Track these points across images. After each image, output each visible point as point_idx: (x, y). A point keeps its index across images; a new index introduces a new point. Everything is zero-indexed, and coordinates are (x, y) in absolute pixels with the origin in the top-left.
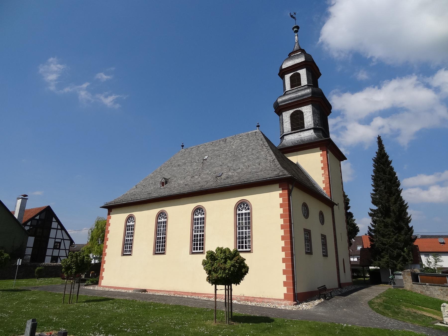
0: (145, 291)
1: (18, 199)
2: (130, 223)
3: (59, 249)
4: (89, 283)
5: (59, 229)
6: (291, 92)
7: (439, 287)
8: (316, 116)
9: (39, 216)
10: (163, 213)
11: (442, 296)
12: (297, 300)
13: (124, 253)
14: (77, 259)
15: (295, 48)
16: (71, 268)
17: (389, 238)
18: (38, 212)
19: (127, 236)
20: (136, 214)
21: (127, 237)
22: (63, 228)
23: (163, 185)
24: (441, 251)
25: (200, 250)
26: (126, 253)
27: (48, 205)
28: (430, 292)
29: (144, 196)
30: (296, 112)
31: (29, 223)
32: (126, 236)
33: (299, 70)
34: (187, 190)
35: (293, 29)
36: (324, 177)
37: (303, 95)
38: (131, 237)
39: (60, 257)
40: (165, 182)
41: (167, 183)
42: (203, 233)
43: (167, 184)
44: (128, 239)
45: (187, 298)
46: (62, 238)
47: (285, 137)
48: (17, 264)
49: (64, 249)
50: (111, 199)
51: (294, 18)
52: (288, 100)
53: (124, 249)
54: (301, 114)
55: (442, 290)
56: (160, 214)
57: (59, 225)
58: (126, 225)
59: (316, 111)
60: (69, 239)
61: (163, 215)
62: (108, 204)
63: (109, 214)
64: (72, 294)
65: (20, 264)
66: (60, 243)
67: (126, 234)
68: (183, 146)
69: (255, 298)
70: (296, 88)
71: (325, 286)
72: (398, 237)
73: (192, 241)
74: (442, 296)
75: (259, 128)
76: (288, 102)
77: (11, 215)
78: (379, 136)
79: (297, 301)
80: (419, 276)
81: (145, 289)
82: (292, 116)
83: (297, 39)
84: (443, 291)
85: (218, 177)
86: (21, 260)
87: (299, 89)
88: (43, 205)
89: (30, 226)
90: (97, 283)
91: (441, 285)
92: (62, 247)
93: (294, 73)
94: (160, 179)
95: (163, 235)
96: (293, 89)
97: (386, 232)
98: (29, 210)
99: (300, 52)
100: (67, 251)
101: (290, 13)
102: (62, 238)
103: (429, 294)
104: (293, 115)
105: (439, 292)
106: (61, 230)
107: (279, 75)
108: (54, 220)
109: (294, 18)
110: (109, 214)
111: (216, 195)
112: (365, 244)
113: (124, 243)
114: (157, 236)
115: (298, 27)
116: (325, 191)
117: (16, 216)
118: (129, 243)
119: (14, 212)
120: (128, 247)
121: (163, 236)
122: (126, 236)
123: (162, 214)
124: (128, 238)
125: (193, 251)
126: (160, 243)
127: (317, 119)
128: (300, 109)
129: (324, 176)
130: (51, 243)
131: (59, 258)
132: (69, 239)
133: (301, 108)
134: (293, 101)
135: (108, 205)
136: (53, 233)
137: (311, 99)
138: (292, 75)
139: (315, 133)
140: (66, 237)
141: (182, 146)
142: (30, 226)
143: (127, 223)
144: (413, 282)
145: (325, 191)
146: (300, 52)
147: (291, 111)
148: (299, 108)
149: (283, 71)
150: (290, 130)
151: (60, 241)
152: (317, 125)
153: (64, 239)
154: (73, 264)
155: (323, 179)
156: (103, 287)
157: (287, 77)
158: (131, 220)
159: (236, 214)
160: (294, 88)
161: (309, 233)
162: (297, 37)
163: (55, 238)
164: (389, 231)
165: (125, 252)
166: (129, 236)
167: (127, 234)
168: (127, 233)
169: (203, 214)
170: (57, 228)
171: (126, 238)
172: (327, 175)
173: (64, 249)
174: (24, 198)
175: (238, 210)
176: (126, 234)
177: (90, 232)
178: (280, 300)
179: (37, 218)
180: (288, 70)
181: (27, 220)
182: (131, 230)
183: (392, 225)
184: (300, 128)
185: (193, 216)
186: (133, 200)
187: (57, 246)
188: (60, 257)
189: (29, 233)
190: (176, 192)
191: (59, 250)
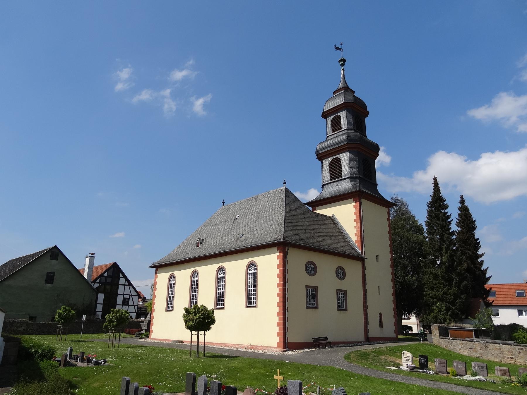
0: (182, 342)
1: (87, 258)
2: (252, 271)
3: (128, 305)
4: (143, 336)
5: (127, 285)
6: (332, 137)
7: (459, 341)
9: (107, 272)
10: (253, 263)
11: (463, 350)
12: (287, 348)
13: (168, 309)
14: (116, 314)
16: (113, 322)
17: (437, 291)
18: (107, 268)
19: (219, 288)
20: (177, 273)
21: (219, 290)
22: (130, 284)
23: (198, 246)
24: (502, 304)
25: (253, 304)
26: (169, 309)
27: (111, 262)
28: (453, 346)
29: (181, 258)
30: (333, 161)
31: (98, 281)
34: (218, 250)
35: (339, 62)
36: (356, 230)
37: (339, 142)
38: (223, 290)
40: (200, 242)
41: (202, 244)
42: (223, 291)
43: (202, 245)
44: (220, 292)
47: (326, 187)
48: (83, 319)
49: (133, 305)
50: (157, 259)
51: (339, 49)
52: (326, 147)
53: (217, 303)
54: (339, 161)
55: (463, 344)
56: (250, 265)
58: (192, 280)
59: (354, 158)
60: (137, 295)
61: (173, 277)
62: (155, 264)
63: (156, 273)
64: (114, 343)
65: (85, 319)
66: (129, 299)
67: (218, 287)
68: (223, 203)
69: (258, 346)
70: (336, 132)
71: (327, 337)
72: (448, 290)
73: (247, 295)
74: (463, 350)
76: (326, 150)
77: (79, 274)
78: (435, 176)
79: (287, 348)
80: (449, 331)
81: (183, 340)
82: (331, 164)
83: (343, 74)
84: (464, 345)
86: (85, 316)
87: (339, 134)
88: (110, 261)
89: (99, 283)
90: (147, 337)
91: (462, 339)
92: (131, 303)
93: (335, 116)
94: (196, 239)
95: (254, 287)
96: (333, 133)
97: (435, 284)
98: (98, 267)
99: (344, 91)
100: (136, 307)
101: (335, 45)
103: (453, 348)
104: (331, 163)
105: (460, 347)
106: (128, 286)
107: (322, 117)
108: (121, 276)
109: (339, 49)
110: (156, 273)
112: (498, 294)
113: (168, 299)
114: (192, 294)
115: (344, 61)
116: (356, 244)
117: (85, 276)
118: (252, 294)
119: (83, 270)
120: (251, 298)
121: (254, 288)
122: (218, 289)
123: (221, 270)
125: (217, 307)
126: (251, 296)
128: (336, 156)
129: (356, 228)
130: (120, 300)
132: (137, 295)
133: (339, 155)
134: (331, 148)
135: (154, 265)
136: (121, 289)
137: (347, 146)
138: (333, 118)
140: (134, 293)
141: (222, 203)
142: (99, 283)
143: (218, 274)
144: (440, 336)
145: (356, 244)
146: (344, 91)
147: (330, 159)
148: (338, 156)
149: (325, 114)
150: (329, 179)
151: (128, 297)
152: (354, 173)
153: (132, 295)
154: (114, 318)
155: (355, 231)
156: (153, 339)
157: (329, 119)
158: (222, 272)
159: (247, 274)
161: (315, 289)
162: (343, 71)
163: (124, 294)
164: (439, 283)
165: (168, 308)
166: (221, 288)
167: (219, 287)
169: (256, 269)
170: (124, 284)
171: (218, 291)
173: (133, 305)
174: (92, 256)
175: (249, 270)
176: (218, 287)
177: (152, 288)
178: (274, 347)
179: (106, 274)
180: (333, 111)
181: (96, 277)
182: (223, 283)
183: (443, 277)
184: (337, 178)
185: (192, 279)
186: (173, 261)
187: (126, 302)
189: (98, 291)
190: (205, 253)
191: (128, 306)
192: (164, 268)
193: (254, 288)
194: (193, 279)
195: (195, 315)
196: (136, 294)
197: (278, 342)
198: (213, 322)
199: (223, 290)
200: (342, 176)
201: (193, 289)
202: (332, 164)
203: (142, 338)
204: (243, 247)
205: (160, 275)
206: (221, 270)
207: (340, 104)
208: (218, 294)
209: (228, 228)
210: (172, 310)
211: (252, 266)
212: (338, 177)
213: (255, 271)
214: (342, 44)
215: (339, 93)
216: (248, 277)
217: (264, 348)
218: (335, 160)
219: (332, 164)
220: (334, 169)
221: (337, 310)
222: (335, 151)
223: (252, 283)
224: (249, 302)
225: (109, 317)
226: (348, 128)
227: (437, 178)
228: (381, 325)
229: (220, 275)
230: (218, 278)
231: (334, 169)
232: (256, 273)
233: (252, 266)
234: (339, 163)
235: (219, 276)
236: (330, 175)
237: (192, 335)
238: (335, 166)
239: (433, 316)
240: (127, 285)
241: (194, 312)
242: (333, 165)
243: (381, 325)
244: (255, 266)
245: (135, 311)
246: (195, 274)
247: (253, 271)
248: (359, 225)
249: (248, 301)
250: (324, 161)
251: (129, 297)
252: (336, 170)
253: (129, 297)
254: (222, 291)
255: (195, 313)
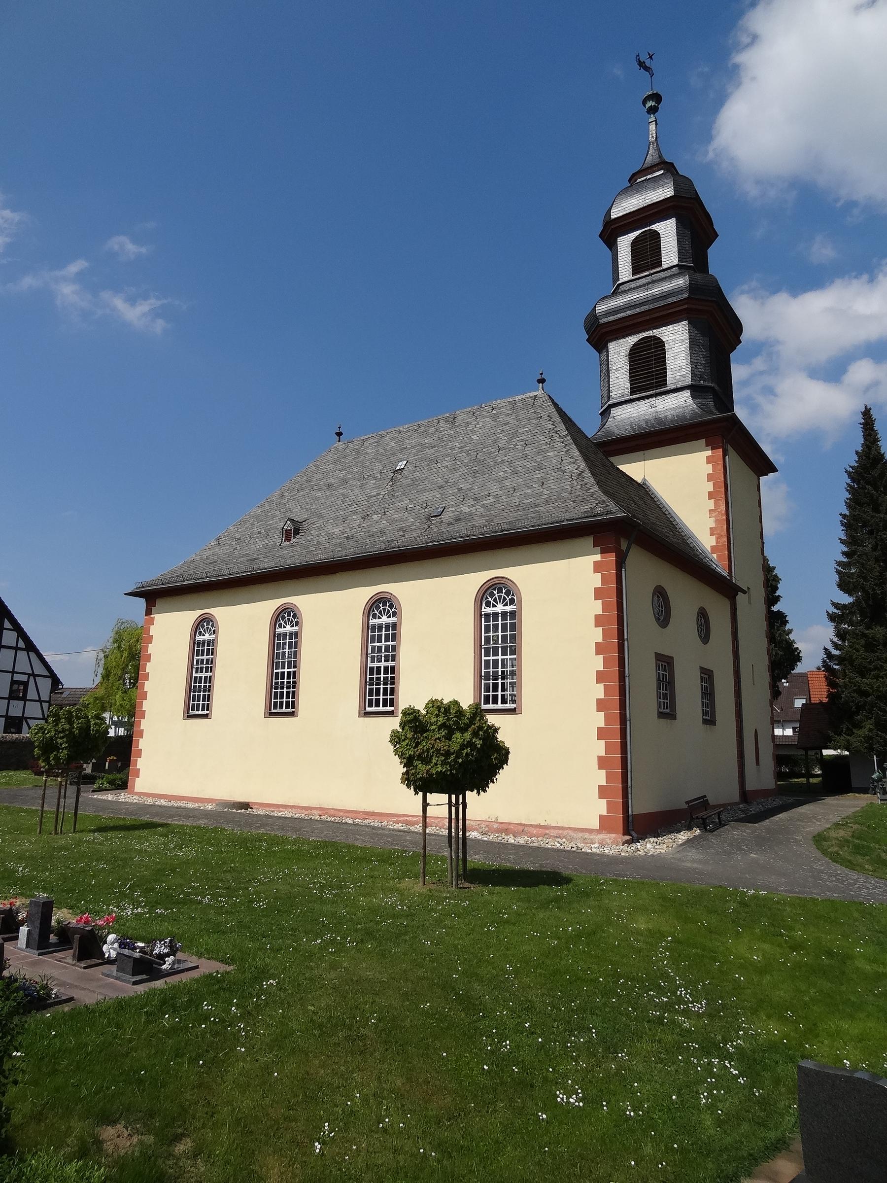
0: (246, 806)
2: (204, 635)
3: (24, 699)
4: (102, 784)
5: (21, 649)
6: (633, 285)
8: (701, 353)
10: (289, 610)
15: (649, 158)
19: (197, 668)
20: (225, 615)
21: (197, 672)
22: (30, 647)
23: (288, 539)
25: (385, 705)
29: (239, 568)
30: (641, 344)
32: (194, 670)
33: (657, 224)
35: (644, 103)
36: (713, 519)
39: (28, 720)
40: (294, 530)
41: (298, 534)
45: (354, 824)
46: (31, 672)
49: (38, 699)
50: (874, 414)
51: (647, 69)
56: (201, 624)
57: (20, 638)
58: (195, 640)
63: (148, 612)
66: (26, 684)
68: (339, 434)
69: (524, 825)
71: (705, 796)
73: (366, 682)
75: (543, 387)
78: (866, 407)
81: (247, 801)
82: (634, 354)
83: (654, 132)
85: (432, 517)
87: (655, 277)
90: (123, 785)
92: (32, 694)
93: (642, 233)
94: (280, 523)
96: (638, 276)
97: (870, 663)
101: (638, 56)
102: (31, 672)
108: (7, 624)
109: (647, 69)
110: (148, 612)
111: (428, 565)
114: (275, 671)
115: (657, 98)
116: (715, 556)
122: (194, 670)
123: (286, 614)
124: (199, 675)
125: (369, 709)
126: (282, 688)
127: (700, 361)
129: (713, 515)
131: (24, 723)
137: (686, 306)
139: (696, 399)
140: (39, 669)
141: (337, 434)
145: (715, 556)
147: (632, 340)
148: (654, 331)
151: (24, 678)
152: (701, 378)
153: (35, 676)
155: (711, 523)
157: (625, 243)
158: (208, 628)
160: (641, 275)
162: (654, 125)
163: (13, 672)
164: (879, 659)
166: (202, 668)
167: (197, 663)
168: (198, 661)
169: (297, 624)
171: (370, 665)
172: (722, 514)
176: (195, 663)
178: (590, 831)
188: (28, 720)
192: (169, 599)
193: (283, 670)
194: (199, 638)
195: (448, 737)
196: (46, 673)
197: (605, 813)
198: (506, 761)
199: (207, 671)
200: (666, 384)
201: (278, 658)
202: (638, 353)
203: (99, 790)
204: (469, 536)
205: (159, 618)
206: (286, 614)
207: (623, 215)
208: (277, 678)
209: (379, 494)
210: (207, 715)
211: (205, 624)
212: (657, 387)
213: (213, 637)
214: (651, 57)
215: (649, 177)
216: (196, 648)
217: (554, 833)
218: (645, 343)
219: (638, 353)
220: (644, 366)
221: (659, 717)
222: (648, 318)
223: (381, 652)
224: (193, 705)
225: (43, 733)
226: (680, 263)
227: (872, 412)
228: (758, 763)
229: (202, 637)
230: (195, 643)
231: (644, 366)
232: (213, 640)
233: (205, 624)
234: (660, 350)
235: (373, 621)
236: (631, 381)
237: (428, 808)
238: (644, 359)
239: (864, 738)
240: (21, 649)
241: (443, 726)
242: (638, 356)
243: (758, 763)
244: (294, 616)
245: (43, 714)
246: (204, 623)
247: (207, 637)
248: (723, 508)
249: (191, 703)
250: (612, 346)
251: (29, 678)
252: (650, 369)
253: (29, 678)
254: (203, 675)
255: (449, 731)
